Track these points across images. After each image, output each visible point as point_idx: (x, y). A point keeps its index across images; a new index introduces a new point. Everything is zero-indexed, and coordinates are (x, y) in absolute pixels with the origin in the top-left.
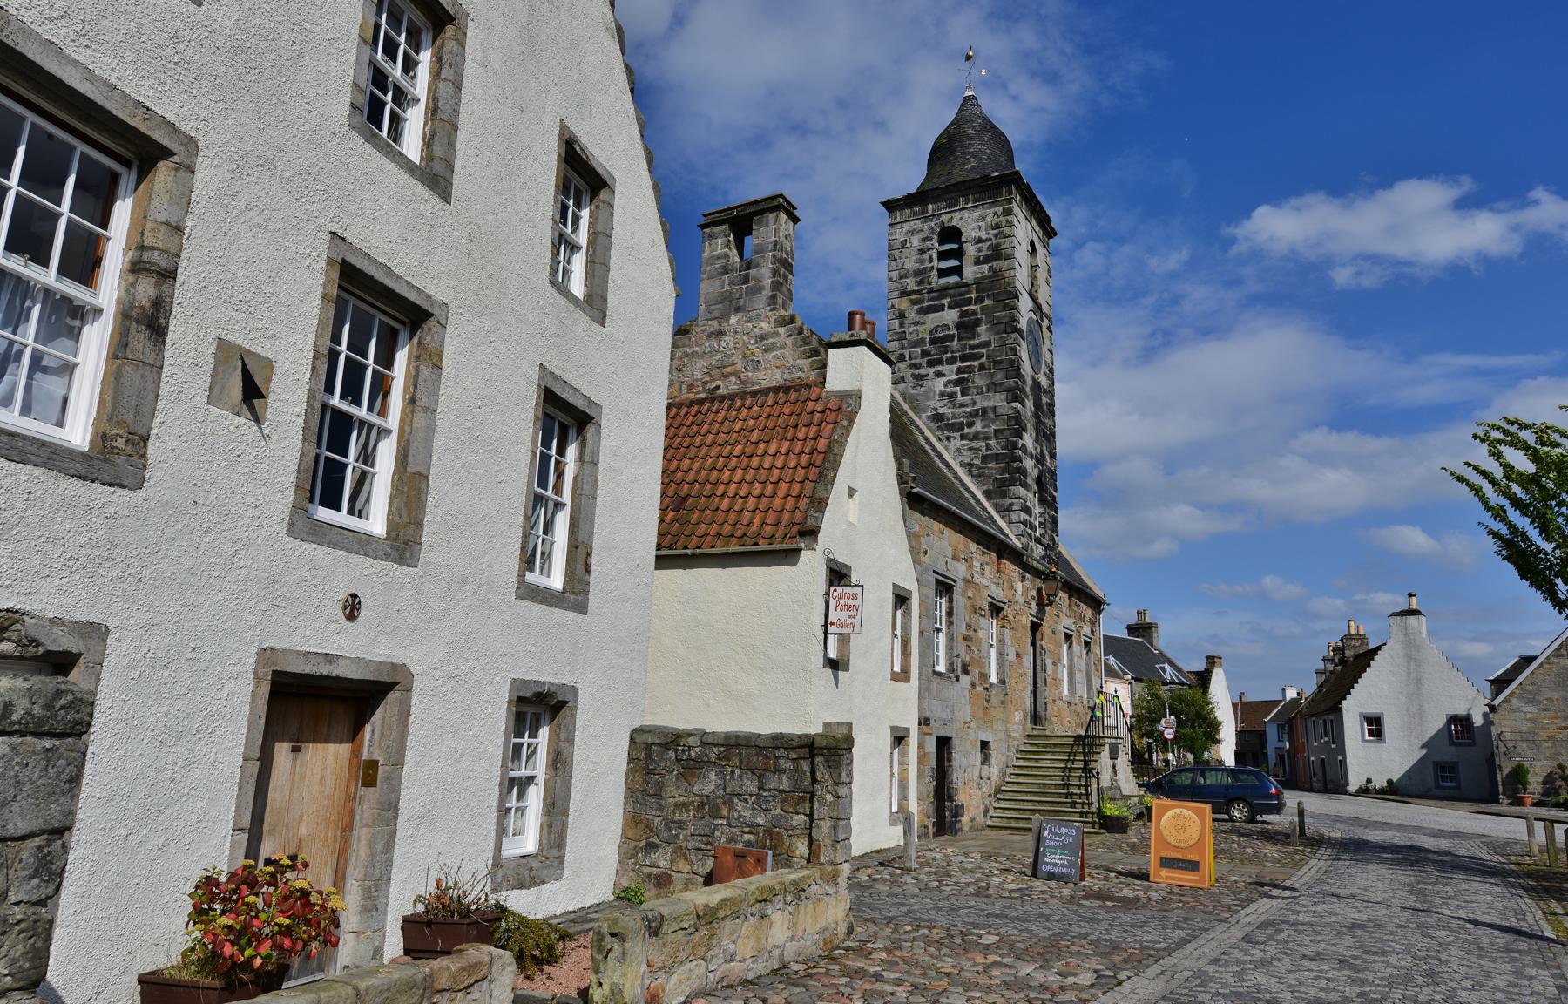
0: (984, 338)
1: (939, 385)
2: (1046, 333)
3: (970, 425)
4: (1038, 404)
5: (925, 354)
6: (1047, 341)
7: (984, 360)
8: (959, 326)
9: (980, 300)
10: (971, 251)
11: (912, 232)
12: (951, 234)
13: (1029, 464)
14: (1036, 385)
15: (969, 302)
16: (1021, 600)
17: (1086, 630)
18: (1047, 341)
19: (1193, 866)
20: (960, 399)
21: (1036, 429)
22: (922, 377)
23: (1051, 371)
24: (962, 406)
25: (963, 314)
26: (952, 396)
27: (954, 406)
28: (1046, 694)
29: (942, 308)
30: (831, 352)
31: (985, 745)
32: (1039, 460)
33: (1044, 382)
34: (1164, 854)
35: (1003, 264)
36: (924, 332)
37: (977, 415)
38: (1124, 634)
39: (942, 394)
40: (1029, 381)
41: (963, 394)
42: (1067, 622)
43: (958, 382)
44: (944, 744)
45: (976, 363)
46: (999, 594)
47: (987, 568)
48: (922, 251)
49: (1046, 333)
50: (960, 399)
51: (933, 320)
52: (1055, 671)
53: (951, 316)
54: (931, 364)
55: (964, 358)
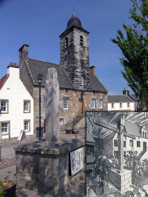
1: (66, 64)
3: (69, 69)
5: (64, 59)
10: (69, 41)
13: (78, 74)
20: (68, 65)
26: (67, 65)
29: (66, 51)
31: (63, 119)
35: (72, 42)
39: (66, 65)
40: (79, 60)
43: (68, 63)
47: (62, 93)
50: (68, 65)
53: (67, 52)
55: (69, 59)
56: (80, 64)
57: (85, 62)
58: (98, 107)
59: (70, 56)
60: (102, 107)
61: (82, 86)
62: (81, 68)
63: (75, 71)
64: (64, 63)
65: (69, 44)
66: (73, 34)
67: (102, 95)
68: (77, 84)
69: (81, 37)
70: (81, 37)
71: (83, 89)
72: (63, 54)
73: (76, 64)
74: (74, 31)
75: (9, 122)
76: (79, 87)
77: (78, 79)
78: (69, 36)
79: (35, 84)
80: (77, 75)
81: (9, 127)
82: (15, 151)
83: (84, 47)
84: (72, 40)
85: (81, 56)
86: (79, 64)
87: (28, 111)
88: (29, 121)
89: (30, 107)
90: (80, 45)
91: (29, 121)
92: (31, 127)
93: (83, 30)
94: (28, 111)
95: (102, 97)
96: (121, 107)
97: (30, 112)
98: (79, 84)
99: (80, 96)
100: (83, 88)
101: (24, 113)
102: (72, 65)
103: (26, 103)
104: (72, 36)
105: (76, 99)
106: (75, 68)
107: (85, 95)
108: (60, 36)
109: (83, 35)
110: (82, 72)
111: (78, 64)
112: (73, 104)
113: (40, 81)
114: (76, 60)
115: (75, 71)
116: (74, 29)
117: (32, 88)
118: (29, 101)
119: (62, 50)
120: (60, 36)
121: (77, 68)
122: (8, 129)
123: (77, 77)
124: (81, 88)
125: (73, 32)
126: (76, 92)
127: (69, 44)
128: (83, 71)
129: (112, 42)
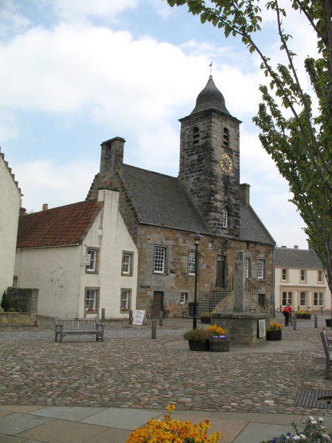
1: (192, 180)
3: (200, 193)
5: (189, 169)
8: (198, 160)
10: (202, 135)
12: (196, 129)
13: (219, 204)
15: (200, 152)
22: (188, 177)
26: (195, 183)
31: (186, 294)
40: (221, 176)
43: (198, 179)
47: (187, 241)
48: (189, 136)
53: (196, 157)
55: (199, 171)
56: (222, 185)
57: (231, 181)
58: (254, 276)
60: (262, 278)
61: (224, 229)
62: (223, 194)
63: (212, 198)
64: (188, 177)
65: (201, 142)
66: (211, 126)
67: (263, 249)
68: (215, 224)
69: (226, 130)
70: (226, 130)
71: (226, 236)
72: (186, 157)
73: (215, 185)
74: (213, 120)
75: (97, 290)
76: (219, 233)
77: (218, 216)
78: (201, 126)
79: (141, 222)
80: (216, 207)
81: (98, 299)
82: (187, 341)
83: (230, 149)
84: (208, 136)
85: (224, 169)
86: (221, 184)
87: (128, 273)
88: (130, 291)
89: (131, 265)
90: (222, 146)
91: (130, 291)
92: (132, 303)
93: (231, 116)
94: (128, 273)
95: (264, 256)
96: (303, 278)
97: (131, 274)
98: (219, 224)
99: (220, 250)
101: (122, 275)
102: (206, 185)
103: (127, 256)
104: (209, 128)
105: (213, 255)
106: (213, 193)
107: (230, 248)
108: (180, 120)
109: (228, 127)
110: (225, 202)
111: (219, 184)
112: (207, 266)
113: (197, 242)
114: (216, 177)
115: (212, 198)
116: (213, 113)
117: (136, 228)
118: (131, 254)
119: (184, 150)
120: (180, 120)
121: (217, 193)
122: (95, 302)
124: (223, 234)
125: (211, 122)
126: (212, 242)
127: (201, 142)
128: (227, 198)
129: (200, 86)
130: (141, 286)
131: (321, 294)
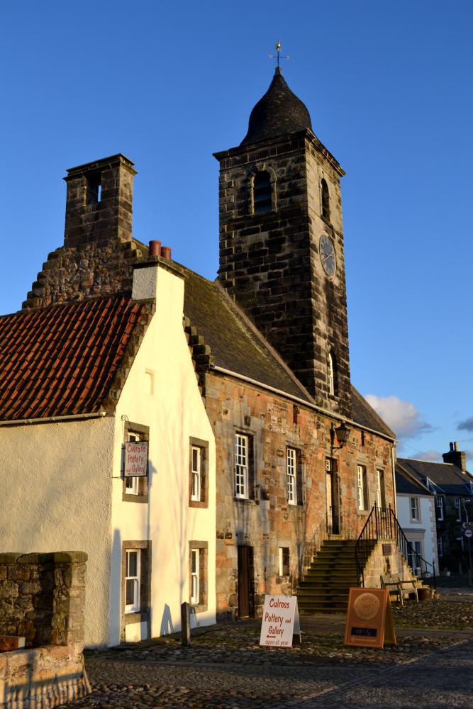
0: (287, 252)
2: (337, 245)
3: (278, 316)
4: (330, 298)
6: (339, 252)
7: (287, 268)
8: (268, 243)
9: (283, 224)
11: (236, 176)
14: (329, 285)
15: (276, 226)
16: (317, 442)
17: (379, 461)
18: (339, 252)
19: (373, 633)
20: (271, 297)
21: (329, 317)
23: (343, 273)
24: (272, 302)
25: (271, 235)
26: (266, 294)
27: (267, 302)
28: (343, 509)
30: (137, 272)
32: (332, 339)
33: (336, 282)
34: (355, 625)
35: (299, 198)
36: (245, 248)
37: (283, 309)
38: (441, 461)
39: (259, 293)
40: (322, 282)
41: (274, 292)
42: (360, 456)
44: (246, 553)
45: (281, 270)
46: (296, 439)
47: (284, 421)
49: (337, 245)
50: (271, 297)
51: (250, 239)
52: (350, 493)
53: (264, 236)
54: (250, 272)
55: (274, 267)
59: (284, 258)
80: (319, 349)
97: (204, 498)
100: (336, 411)
120: (219, 156)
123: (320, 359)
125: (303, 160)
130: (219, 536)
131: (417, 544)
